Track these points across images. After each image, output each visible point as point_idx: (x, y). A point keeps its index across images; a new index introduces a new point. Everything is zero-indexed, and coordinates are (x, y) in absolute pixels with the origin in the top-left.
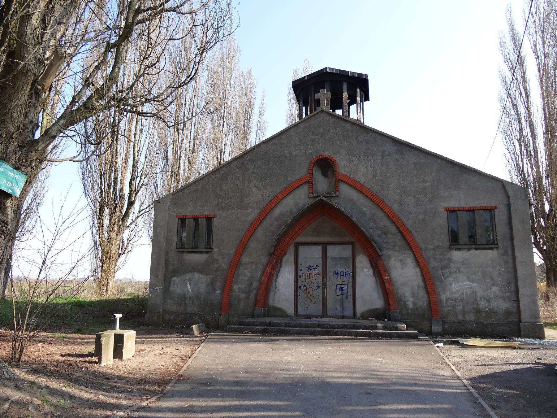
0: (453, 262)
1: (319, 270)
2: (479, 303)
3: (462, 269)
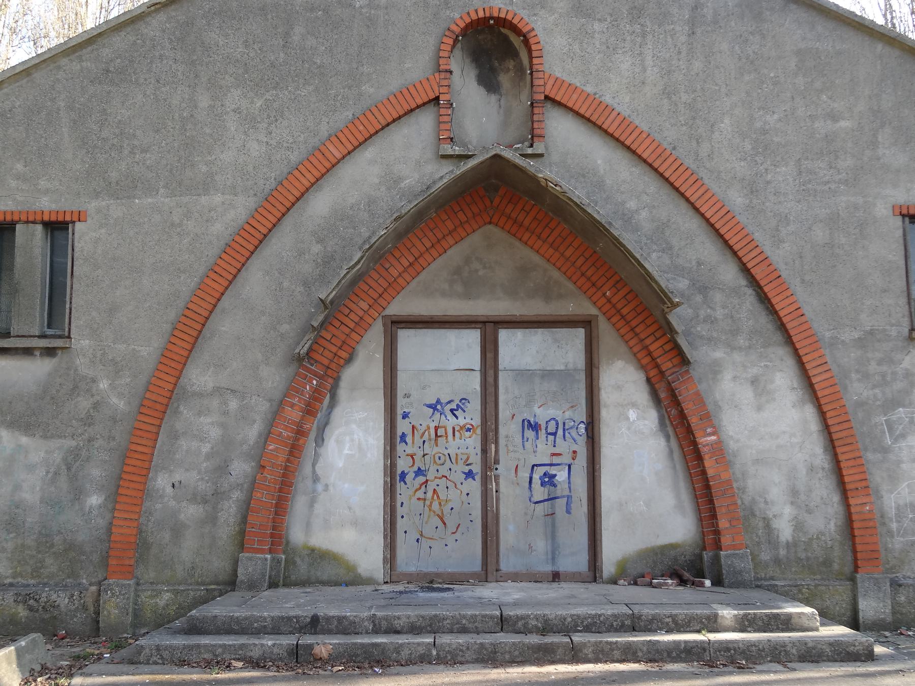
1: (472, 415)
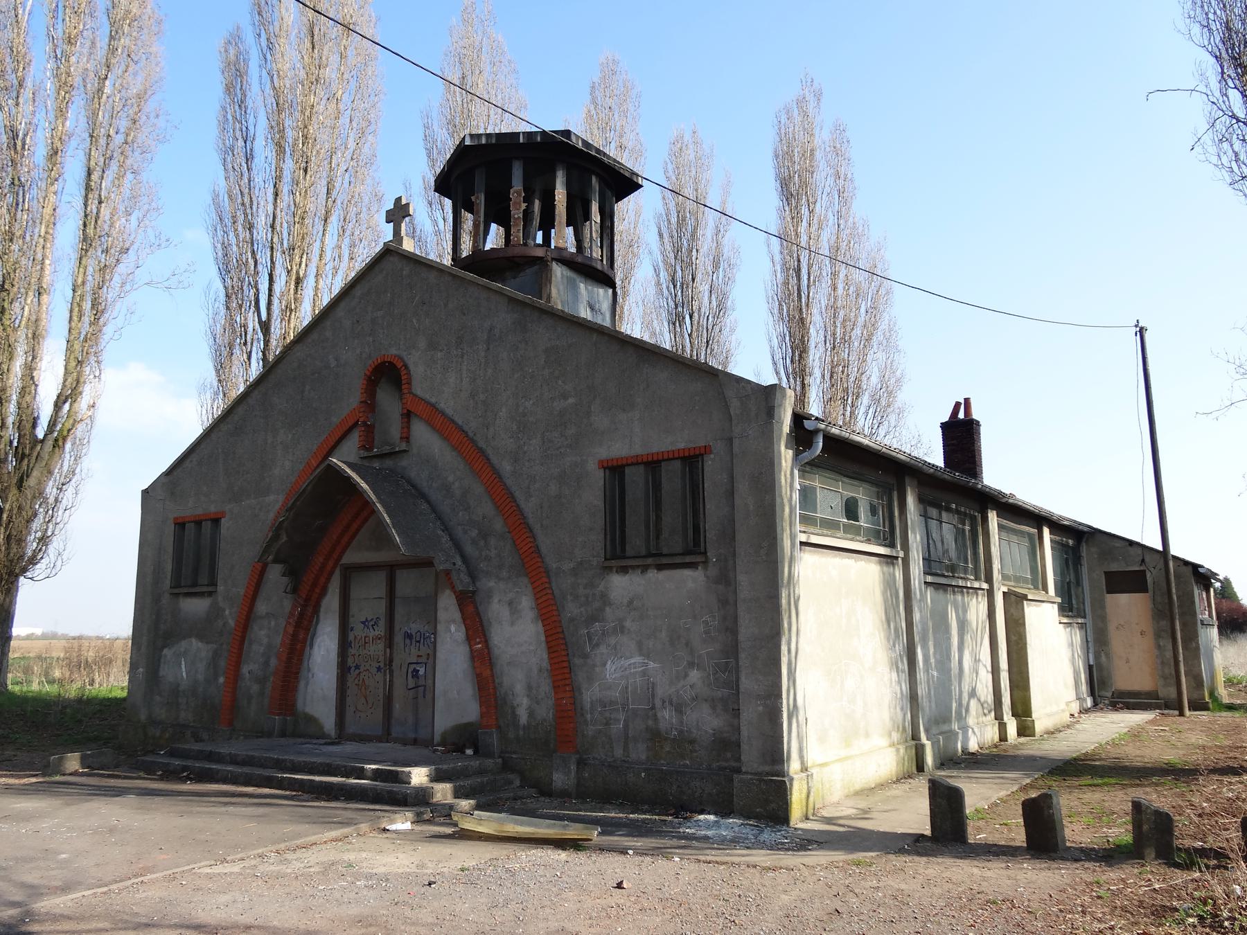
0: (610, 604)
1: (380, 630)
2: (659, 715)
3: (628, 624)
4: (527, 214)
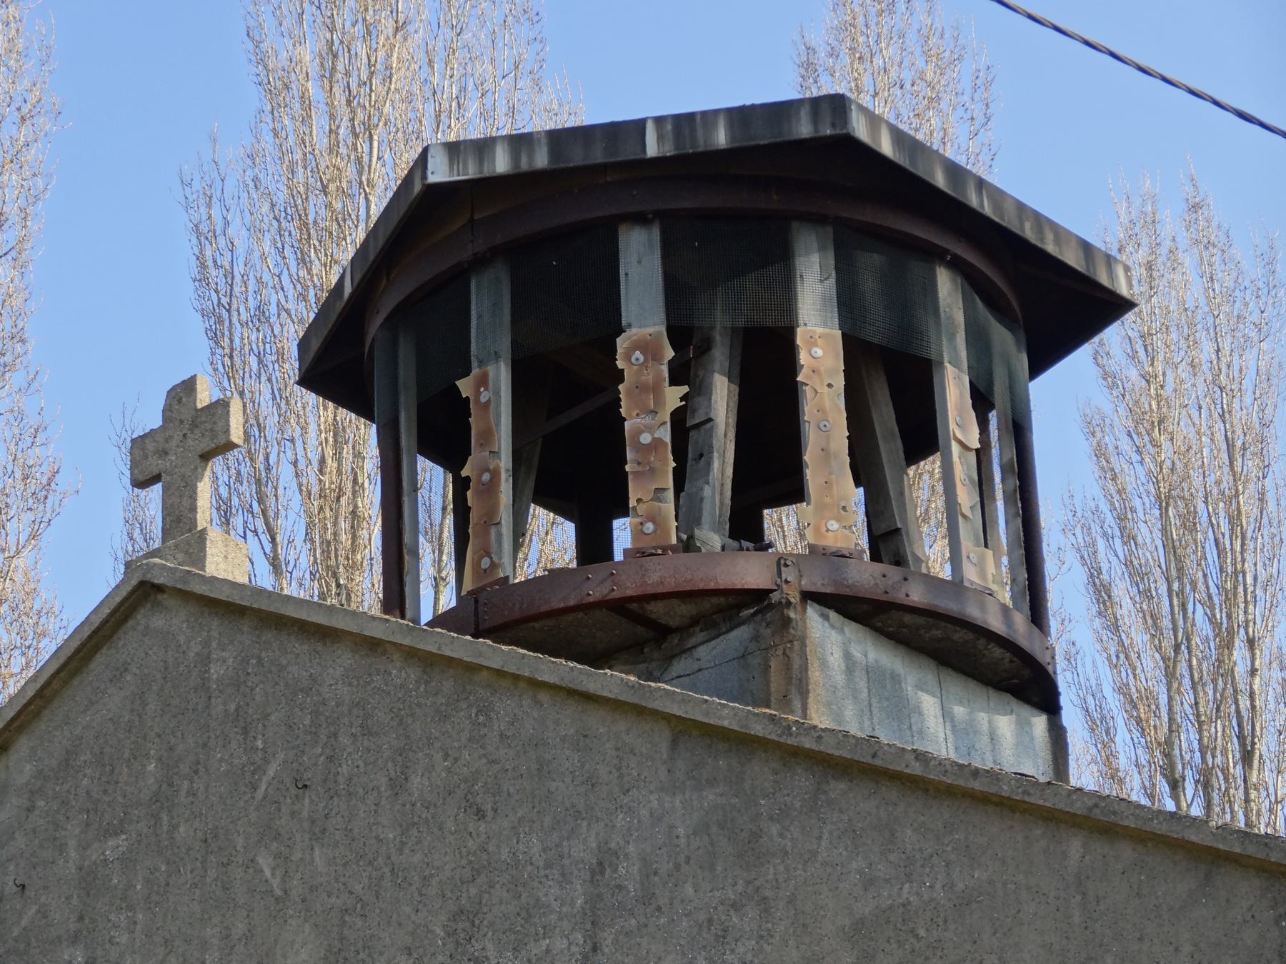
4: (686, 430)
